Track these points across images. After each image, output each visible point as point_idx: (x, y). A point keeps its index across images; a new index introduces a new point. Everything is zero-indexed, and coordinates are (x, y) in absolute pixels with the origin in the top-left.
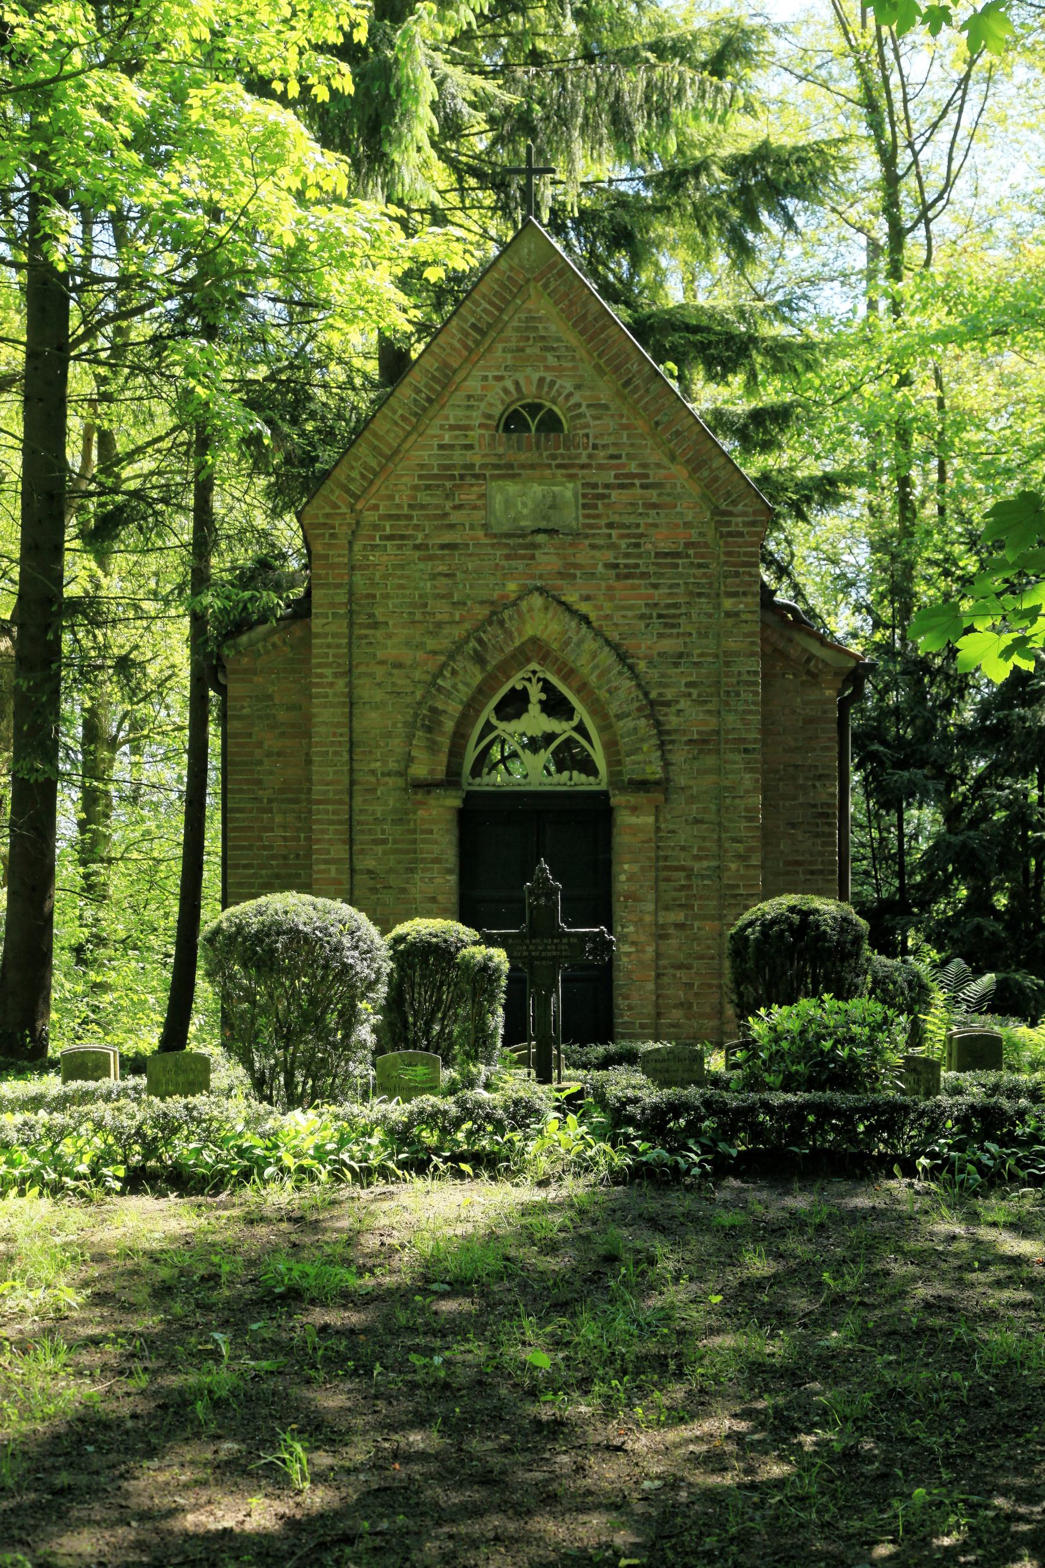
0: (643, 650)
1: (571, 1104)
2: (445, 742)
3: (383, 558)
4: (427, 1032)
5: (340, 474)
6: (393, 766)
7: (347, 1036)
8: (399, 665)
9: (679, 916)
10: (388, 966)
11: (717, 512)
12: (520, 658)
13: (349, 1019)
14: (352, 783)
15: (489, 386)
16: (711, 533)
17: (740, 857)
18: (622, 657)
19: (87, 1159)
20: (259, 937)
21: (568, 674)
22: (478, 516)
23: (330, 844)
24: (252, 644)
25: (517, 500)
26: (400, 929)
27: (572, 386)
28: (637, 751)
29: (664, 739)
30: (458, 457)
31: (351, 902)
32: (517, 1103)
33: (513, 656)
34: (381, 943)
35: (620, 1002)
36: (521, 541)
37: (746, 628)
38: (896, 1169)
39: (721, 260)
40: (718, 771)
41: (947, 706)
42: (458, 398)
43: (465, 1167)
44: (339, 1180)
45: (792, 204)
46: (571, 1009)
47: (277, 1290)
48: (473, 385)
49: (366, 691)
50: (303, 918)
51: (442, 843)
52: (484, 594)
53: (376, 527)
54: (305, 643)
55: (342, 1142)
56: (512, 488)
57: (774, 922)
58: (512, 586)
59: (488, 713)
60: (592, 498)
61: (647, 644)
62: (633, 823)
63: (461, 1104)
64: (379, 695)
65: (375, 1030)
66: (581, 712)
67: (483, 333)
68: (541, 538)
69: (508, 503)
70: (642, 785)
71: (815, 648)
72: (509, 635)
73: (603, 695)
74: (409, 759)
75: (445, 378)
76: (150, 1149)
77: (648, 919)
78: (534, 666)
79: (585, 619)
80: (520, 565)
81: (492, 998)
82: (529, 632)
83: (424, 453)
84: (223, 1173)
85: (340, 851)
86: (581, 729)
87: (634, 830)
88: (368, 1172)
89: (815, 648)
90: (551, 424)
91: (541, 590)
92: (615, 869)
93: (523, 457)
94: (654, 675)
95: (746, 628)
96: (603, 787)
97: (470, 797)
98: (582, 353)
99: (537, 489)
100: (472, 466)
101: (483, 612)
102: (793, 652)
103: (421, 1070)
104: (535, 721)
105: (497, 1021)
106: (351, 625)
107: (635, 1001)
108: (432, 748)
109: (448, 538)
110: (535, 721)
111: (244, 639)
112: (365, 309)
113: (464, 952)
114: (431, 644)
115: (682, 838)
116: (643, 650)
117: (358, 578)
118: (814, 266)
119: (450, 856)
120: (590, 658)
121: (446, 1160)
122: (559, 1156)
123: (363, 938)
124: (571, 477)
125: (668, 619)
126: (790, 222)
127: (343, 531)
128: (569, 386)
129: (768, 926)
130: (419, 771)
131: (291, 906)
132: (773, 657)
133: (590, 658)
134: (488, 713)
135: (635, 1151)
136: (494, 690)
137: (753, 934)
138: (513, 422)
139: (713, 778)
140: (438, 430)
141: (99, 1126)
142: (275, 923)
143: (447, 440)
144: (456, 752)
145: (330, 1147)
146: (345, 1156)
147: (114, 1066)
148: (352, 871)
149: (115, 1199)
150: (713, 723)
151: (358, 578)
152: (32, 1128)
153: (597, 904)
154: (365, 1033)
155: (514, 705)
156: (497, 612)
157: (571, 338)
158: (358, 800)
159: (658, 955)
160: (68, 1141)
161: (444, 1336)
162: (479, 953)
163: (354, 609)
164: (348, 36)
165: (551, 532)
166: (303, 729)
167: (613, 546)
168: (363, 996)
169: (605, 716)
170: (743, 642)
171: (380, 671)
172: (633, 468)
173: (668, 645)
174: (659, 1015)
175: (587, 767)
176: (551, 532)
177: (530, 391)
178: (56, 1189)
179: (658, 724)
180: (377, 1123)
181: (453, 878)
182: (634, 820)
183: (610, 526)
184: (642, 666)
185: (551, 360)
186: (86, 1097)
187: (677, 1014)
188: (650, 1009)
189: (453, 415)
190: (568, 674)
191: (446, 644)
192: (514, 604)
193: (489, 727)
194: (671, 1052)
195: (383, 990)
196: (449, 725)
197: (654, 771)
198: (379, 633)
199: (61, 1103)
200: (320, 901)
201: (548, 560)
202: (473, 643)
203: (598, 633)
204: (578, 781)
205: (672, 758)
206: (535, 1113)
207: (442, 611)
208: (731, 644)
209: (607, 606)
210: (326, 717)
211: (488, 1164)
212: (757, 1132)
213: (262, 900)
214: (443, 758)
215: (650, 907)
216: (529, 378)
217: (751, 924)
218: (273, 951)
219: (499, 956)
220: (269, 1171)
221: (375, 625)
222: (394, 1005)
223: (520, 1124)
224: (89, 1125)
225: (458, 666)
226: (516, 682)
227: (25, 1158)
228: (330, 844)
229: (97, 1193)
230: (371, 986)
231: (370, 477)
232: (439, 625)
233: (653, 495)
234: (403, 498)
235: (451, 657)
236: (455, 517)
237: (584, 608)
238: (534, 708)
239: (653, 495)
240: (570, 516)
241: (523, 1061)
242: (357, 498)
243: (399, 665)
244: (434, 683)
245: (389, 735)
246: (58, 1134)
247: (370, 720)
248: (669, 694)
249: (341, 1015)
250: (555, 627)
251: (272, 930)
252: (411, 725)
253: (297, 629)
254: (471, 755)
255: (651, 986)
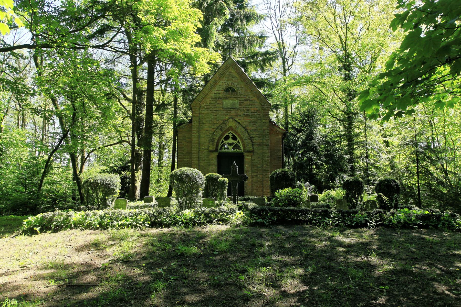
0: (249, 128)
1: (240, 208)
2: (215, 144)
3: (205, 112)
4: (212, 194)
5: (197, 98)
6: (206, 148)
7: (197, 195)
8: (207, 131)
9: (256, 174)
10: (205, 182)
11: (262, 105)
12: (228, 130)
13: (197, 192)
14: (199, 151)
15: (223, 84)
16: (261, 109)
17: (266, 164)
18: (246, 130)
19: (142, 220)
20: (179, 176)
21: (236, 133)
22: (221, 105)
23: (195, 161)
24: (182, 127)
25: (228, 103)
26: (207, 175)
27: (237, 84)
28: (248, 146)
29: (253, 144)
30: (218, 96)
31: (199, 169)
32: (231, 209)
33: (227, 130)
34: (204, 178)
35: (245, 189)
36: (228, 110)
37: (267, 125)
38: (309, 223)
39: (259, 71)
40: (262, 149)
41: (297, 141)
42: (218, 86)
43: (220, 222)
44: (194, 225)
45: (271, 62)
46: (238, 190)
47: (179, 254)
48: (220, 83)
49: (202, 135)
50: (189, 172)
51: (214, 161)
52: (222, 119)
53: (203, 107)
54: (191, 127)
55: (195, 217)
56: (227, 101)
57: (279, 174)
58: (227, 117)
59: (223, 139)
60: (241, 103)
61: (250, 127)
62: (248, 158)
63: (220, 209)
64: (204, 136)
65: (202, 194)
66: (239, 139)
67: (222, 75)
68: (232, 109)
69: (226, 103)
70: (249, 152)
71: (278, 129)
72: (226, 125)
73: (242, 136)
74: (209, 147)
75: (216, 82)
76: (156, 218)
77: (250, 174)
78: (230, 131)
79: (239, 123)
80: (228, 114)
81: (225, 188)
82: (230, 125)
83: (212, 95)
84: (170, 223)
85: (197, 162)
86: (238, 142)
87: (248, 159)
88: (200, 223)
89: (278, 129)
90: (233, 90)
91: (232, 118)
92: (244, 166)
93: (229, 96)
94: (251, 133)
95: (267, 125)
96: (242, 151)
97: (219, 153)
98: (239, 79)
99: (231, 101)
100: (220, 97)
101: (222, 122)
102: (274, 130)
103: (211, 202)
104: (231, 141)
105: (226, 192)
106: (199, 124)
107: (248, 188)
108: (213, 145)
109: (216, 109)
110: (231, 141)
111: (181, 126)
112: (203, 68)
113: (220, 179)
114: (213, 127)
115: (256, 161)
116: (249, 128)
117: (200, 116)
118: (273, 72)
119: (216, 163)
120: (240, 130)
121: (216, 221)
122: (234, 215)
123: (201, 177)
124: (237, 99)
125: (253, 123)
126: (270, 64)
127: (198, 108)
128: (237, 84)
129: (278, 174)
130: (211, 149)
131: (187, 170)
132: (271, 130)
133: (240, 130)
134: (223, 139)
135: (255, 219)
136: (224, 135)
137: (275, 176)
138: (227, 90)
139: (261, 150)
140: (214, 91)
141: (145, 213)
142: (183, 173)
143: (216, 92)
144: (217, 146)
145: (193, 218)
146: (196, 220)
147: (154, 200)
148: (199, 166)
149: (147, 228)
150: (261, 141)
151: (200, 116)
152: (131, 213)
153: (242, 170)
154: (200, 194)
155: (227, 138)
156: (224, 122)
157: (237, 76)
158: (200, 153)
159: (252, 181)
160: (139, 216)
161: (217, 268)
162: (223, 179)
163: (200, 121)
164: (200, 19)
165: (233, 108)
166: (191, 142)
167: (244, 111)
168: (200, 187)
169: (243, 140)
170: (269, 124)
171: (204, 131)
172: (247, 98)
173: (254, 128)
174: (252, 191)
175: (239, 148)
176: (233, 108)
177: (230, 85)
178: (136, 226)
179: (252, 141)
180: (202, 213)
181: (216, 167)
182: (248, 157)
183: (244, 107)
184: (249, 131)
185: (233, 79)
186: (147, 206)
187: (255, 191)
188: (250, 190)
189: (217, 88)
190: (236, 133)
191: (216, 127)
192: (227, 120)
193: (223, 142)
194: (259, 198)
195: (204, 186)
196: (216, 141)
197: (251, 149)
198: (204, 125)
199: (144, 207)
200: (192, 169)
201: (233, 113)
202: (220, 127)
203: (242, 126)
204: (237, 151)
205: (254, 147)
206: (234, 211)
207: (215, 121)
208: (264, 128)
209: (243, 121)
210: (195, 139)
211: (224, 221)
212: (279, 215)
213: (181, 168)
214: (215, 146)
215: (251, 172)
216: (230, 82)
217: (274, 174)
218: (182, 178)
219: (226, 180)
220: (180, 223)
221: (203, 124)
222: (206, 189)
223: (232, 213)
224: (143, 213)
225: (217, 131)
226: (227, 134)
227: (130, 220)
228: (195, 161)
229: (144, 228)
230: (201, 185)
231: (203, 99)
232: (214, 124)
233: (251, 103)
234: (208, 102)
235: (216, 129)
236: (217, 106)
237: (239, 121)
238: (230, 139)
239: (251, 103)
240: (237, 106)
241: (231, 200)
242: (200, 102)
243: (207, 131)
244: (213, 134)
245: (205, 142)
246: (137, 214)
247: (202, 140)
248: (254, 136)
249: (196, 191)
250: (234, 124)
251: (183, 174)
252: (209, 141)
253: (190, 125)
254: (220, 146)
255: (251, 186)
